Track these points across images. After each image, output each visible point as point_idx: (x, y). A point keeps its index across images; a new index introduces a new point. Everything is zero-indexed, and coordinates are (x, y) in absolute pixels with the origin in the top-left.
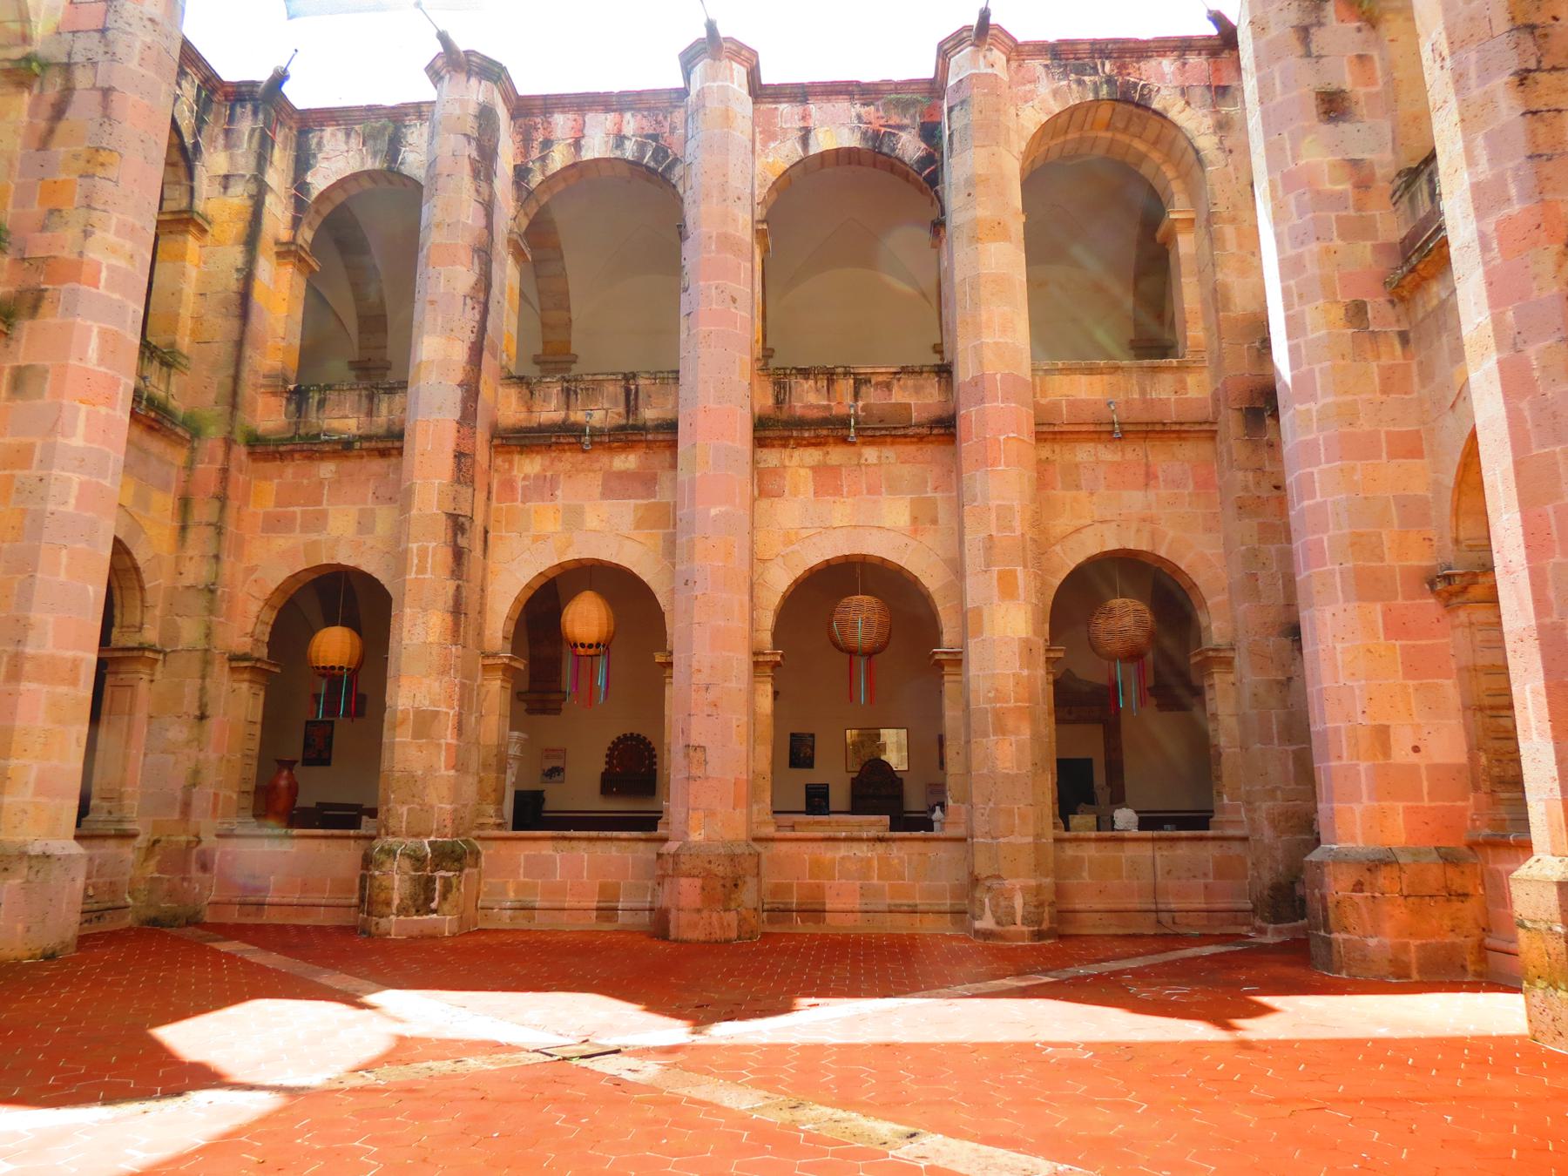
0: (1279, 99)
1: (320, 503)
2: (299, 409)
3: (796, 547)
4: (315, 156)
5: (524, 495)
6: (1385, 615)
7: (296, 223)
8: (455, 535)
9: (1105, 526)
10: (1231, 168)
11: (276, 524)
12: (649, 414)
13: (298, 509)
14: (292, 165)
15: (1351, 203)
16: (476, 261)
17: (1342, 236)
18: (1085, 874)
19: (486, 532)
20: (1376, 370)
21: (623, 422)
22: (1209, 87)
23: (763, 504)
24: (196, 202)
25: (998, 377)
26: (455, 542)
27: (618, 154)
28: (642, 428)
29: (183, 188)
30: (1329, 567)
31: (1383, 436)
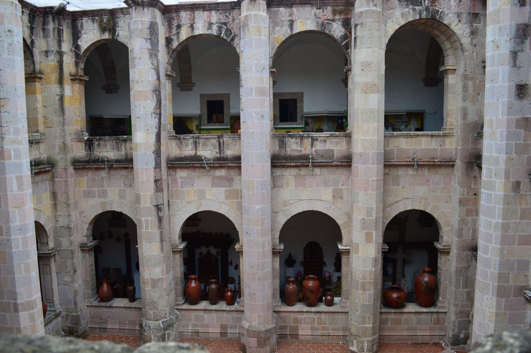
0: (499, 83)
1: (104, 187)
2: (90, 148)
3: (288, 207)
4: (80, 32)
5: (182, 186)
6: (505, 302)
7: (77, 64)
8: (158, 213)
9: (408, 200)
10: (475, 54)
11: (88, 194)
12: (229, 153)
13: (96, 189)
14: (71, 36)
15: (522, 138)
16: (155, 96)
17: (516, 153)
18: (389, 323)
19: (169, 201)
20: (519, 210)
21: (218, 155)
22: (470, 13)
23: (276, 190)
24: (36, 66)
25: (370, 154)
26: (158, 215)
27: (210, 32)
28: (225, 159)
29: (30, 61)
30: (489, 282)
31: (517, 237)
